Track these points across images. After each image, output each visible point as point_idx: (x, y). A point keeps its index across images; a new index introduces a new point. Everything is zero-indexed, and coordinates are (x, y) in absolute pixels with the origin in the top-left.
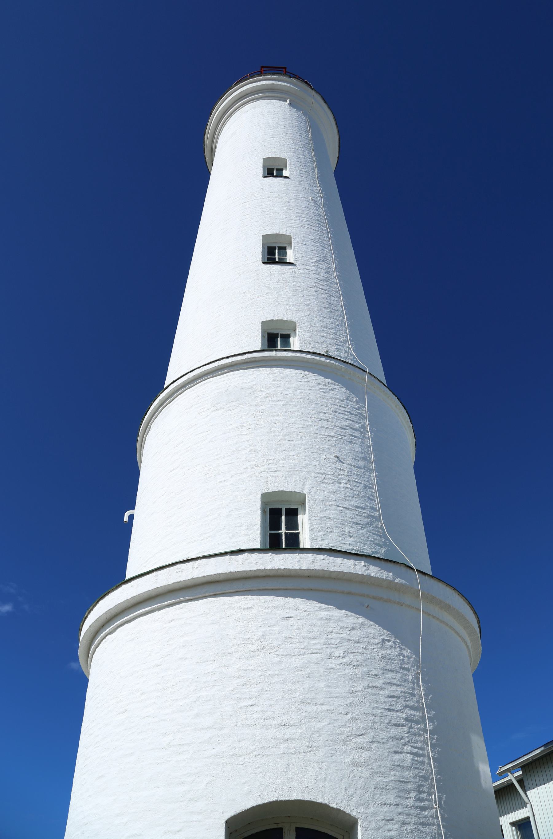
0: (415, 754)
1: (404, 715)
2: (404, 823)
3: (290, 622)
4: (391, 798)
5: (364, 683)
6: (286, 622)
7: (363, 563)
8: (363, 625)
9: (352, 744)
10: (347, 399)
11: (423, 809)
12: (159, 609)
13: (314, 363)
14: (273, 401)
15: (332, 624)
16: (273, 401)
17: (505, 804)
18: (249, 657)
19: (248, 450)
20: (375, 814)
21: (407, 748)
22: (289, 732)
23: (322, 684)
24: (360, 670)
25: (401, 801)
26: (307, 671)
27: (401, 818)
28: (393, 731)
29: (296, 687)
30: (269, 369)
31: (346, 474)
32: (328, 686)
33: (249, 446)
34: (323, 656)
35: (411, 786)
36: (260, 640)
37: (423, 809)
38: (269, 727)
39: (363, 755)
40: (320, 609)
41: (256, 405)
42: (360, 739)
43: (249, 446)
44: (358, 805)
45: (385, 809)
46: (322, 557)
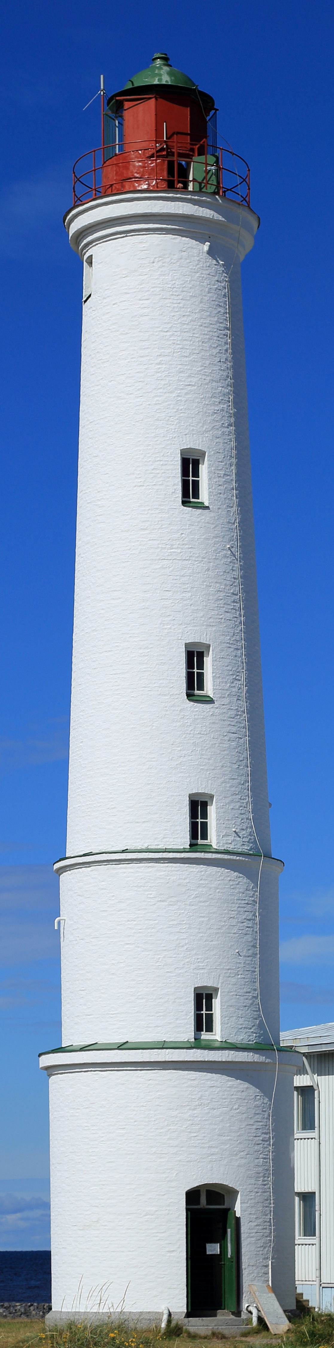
0: (265, 1158)
1: (261, 1138)
2: (257, 1192)
3: (214, 1089)
4: (253, 1181)
5: (246, 1123)
6: (211, 1089)
7: (251, 1054)
8: (247, 1088)
9: (239, 1156)
10: (247, 890)
11: (265, 1185)
12: (141, 1070)
13: (228, 861)
14: (200, 902)
15: (233, 1090)
16: (200, 902)
17: (327, 1065)
18: (194, 1109)
19: (185, 948)
20: (246, 1189)
21: (261, 1156)
22: (213, 1150)
23: (228, 1125)
24: (245, 1116)
25: (256, 1182)
26: (221, 1118)
27: (256, 1190)
28: (256, 1147)
29: (216, 1127)
30: (198, 866)
31: (242, 965)
32: (230, 1126)
33: (186, 944)
34: (228, 1109)
35: (261, 1175)
36: (200, 1098)
37: (265, 1185)
38: (204, 1147)
39: (243, 1161)
40: (228, 1081)
41: (190, 905)
42: (242, 1153)
43: (186, 944)
44: (240, 1185)
45: (250, 1186)
46: (233, 1052)
